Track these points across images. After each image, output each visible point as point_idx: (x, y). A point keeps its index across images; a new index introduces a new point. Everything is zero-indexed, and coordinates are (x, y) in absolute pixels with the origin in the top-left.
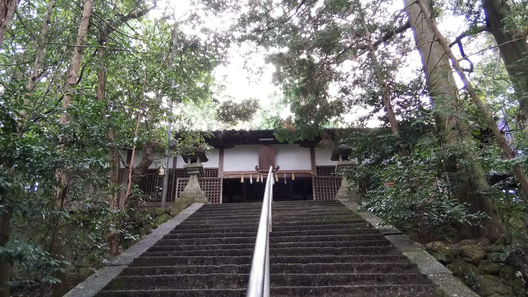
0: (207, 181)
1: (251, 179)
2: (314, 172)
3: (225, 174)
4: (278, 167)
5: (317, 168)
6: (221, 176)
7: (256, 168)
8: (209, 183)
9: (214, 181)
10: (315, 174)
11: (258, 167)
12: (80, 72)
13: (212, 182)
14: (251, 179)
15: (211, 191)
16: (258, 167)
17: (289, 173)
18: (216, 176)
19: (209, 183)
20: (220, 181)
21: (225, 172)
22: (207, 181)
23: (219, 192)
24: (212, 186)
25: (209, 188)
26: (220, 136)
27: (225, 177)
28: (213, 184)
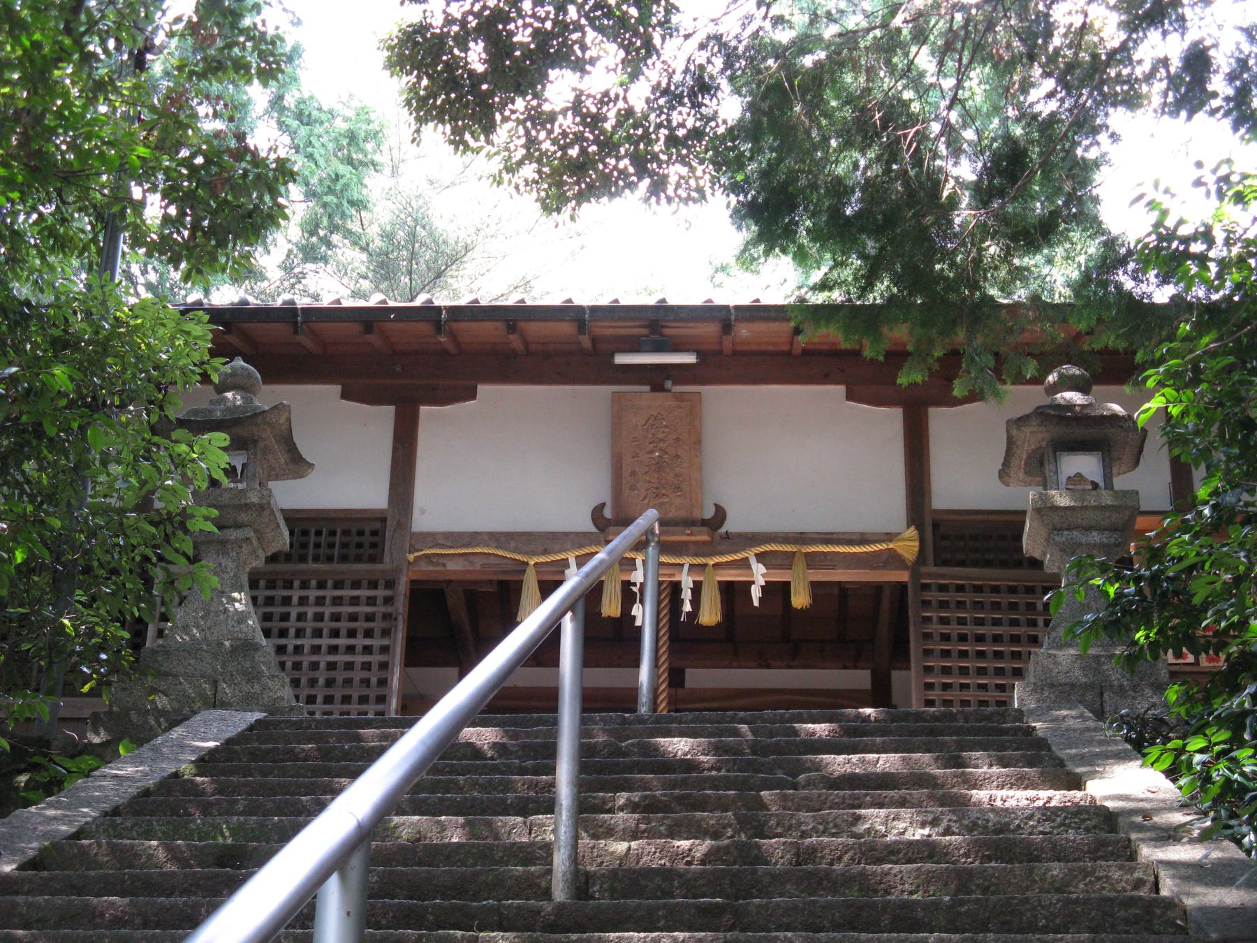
20: (390, 584)
23: (384, 666)
26: (534, 329)
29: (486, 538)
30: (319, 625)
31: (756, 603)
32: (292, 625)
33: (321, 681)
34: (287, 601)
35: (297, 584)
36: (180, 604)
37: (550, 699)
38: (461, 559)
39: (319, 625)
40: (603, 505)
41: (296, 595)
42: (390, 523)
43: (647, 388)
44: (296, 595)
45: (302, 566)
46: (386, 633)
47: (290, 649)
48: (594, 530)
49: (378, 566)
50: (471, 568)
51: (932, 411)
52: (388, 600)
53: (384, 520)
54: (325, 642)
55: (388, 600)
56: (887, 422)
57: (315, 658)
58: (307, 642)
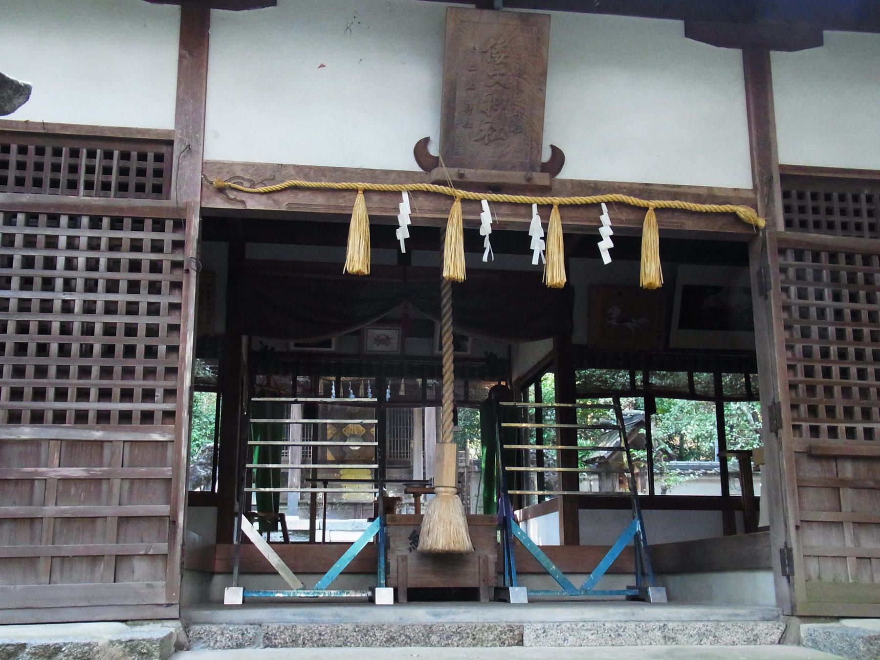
0: (95, 223)
1: (606, 231)
2: (768, 213)
3: (223, 176)
4: (558, 158)
5: (784, 178)
6: (188, 193)
7: (420, 150)
8: (84, 234)
9: (138, 224)
10: (768, 219)
11: (434, 150)
12: (29, 448)
13: (127, 235)
14: (606, 231)
15: (101, 297)
16: (434, 150)
17: (631, 202)
18: (158, 190)
19: (84, 234)
20: (180, 225)
21: (221, 166)
22: (74, 222)
23: (174, 328)
24: (126, 256)
25: (80, 275)
26: (21, 100)
27: (218, 203)
28: (136, 246)
29: (293, 172)
30: (93, 275)
31: (607, 259)
32: (60, 272)
33: (97, 349)
34: (52, 242)
35: (64, 220)
36: (468, 89)
37: (458, 373)
38: (265, 197)
39: (93, 275)
40: (426, 140)
41: (63, 234)
42: (177, 148)
43: (473, 6)
44: (63, 234)
45: (71, 199)
46: (176, 286)
47: (57, 305)
48: (418, 169)
49: (164, 203)
50: (277, 209)
51: (774, 55)
52: (178, 245)
53: (170, 143)
54: (122, 297)
55: (178, 245)
56: (731, 60)
57: (110, 319)
58: (101, 297)
